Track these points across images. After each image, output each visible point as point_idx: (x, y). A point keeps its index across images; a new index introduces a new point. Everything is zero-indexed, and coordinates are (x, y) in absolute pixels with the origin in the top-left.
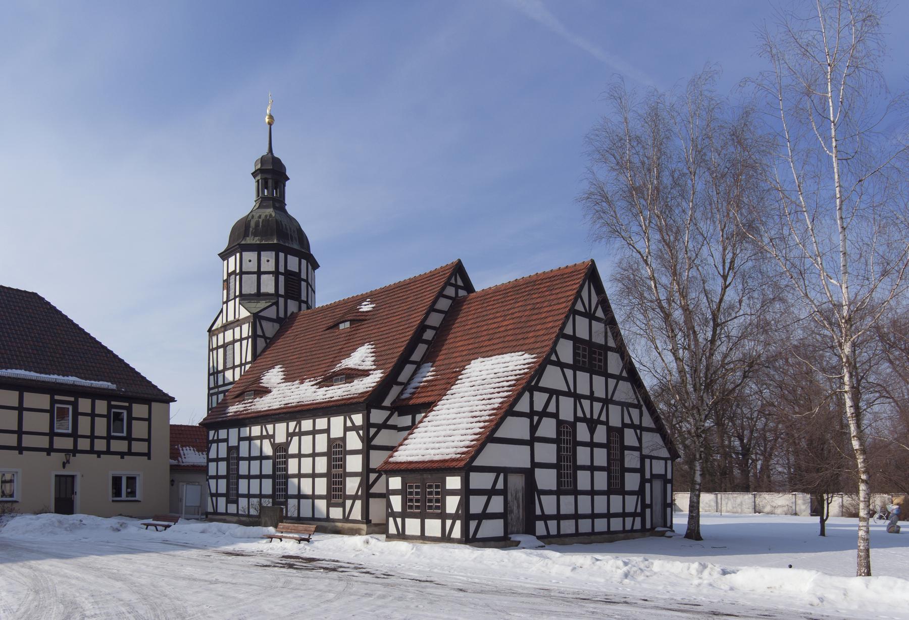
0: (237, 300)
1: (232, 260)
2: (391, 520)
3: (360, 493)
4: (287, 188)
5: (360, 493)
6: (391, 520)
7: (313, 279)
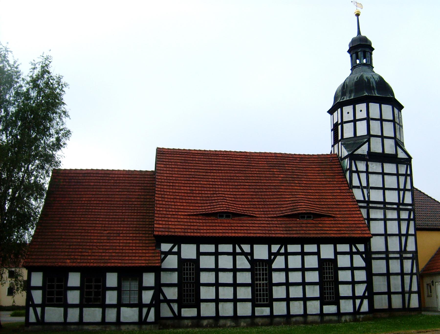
0: (340, 143)
1: (336, 114)
2: (31, 309)
3: (366, 294)
4: (373, 56)
5: (366, 294)
6: (31, 309)
7: (400, 118)
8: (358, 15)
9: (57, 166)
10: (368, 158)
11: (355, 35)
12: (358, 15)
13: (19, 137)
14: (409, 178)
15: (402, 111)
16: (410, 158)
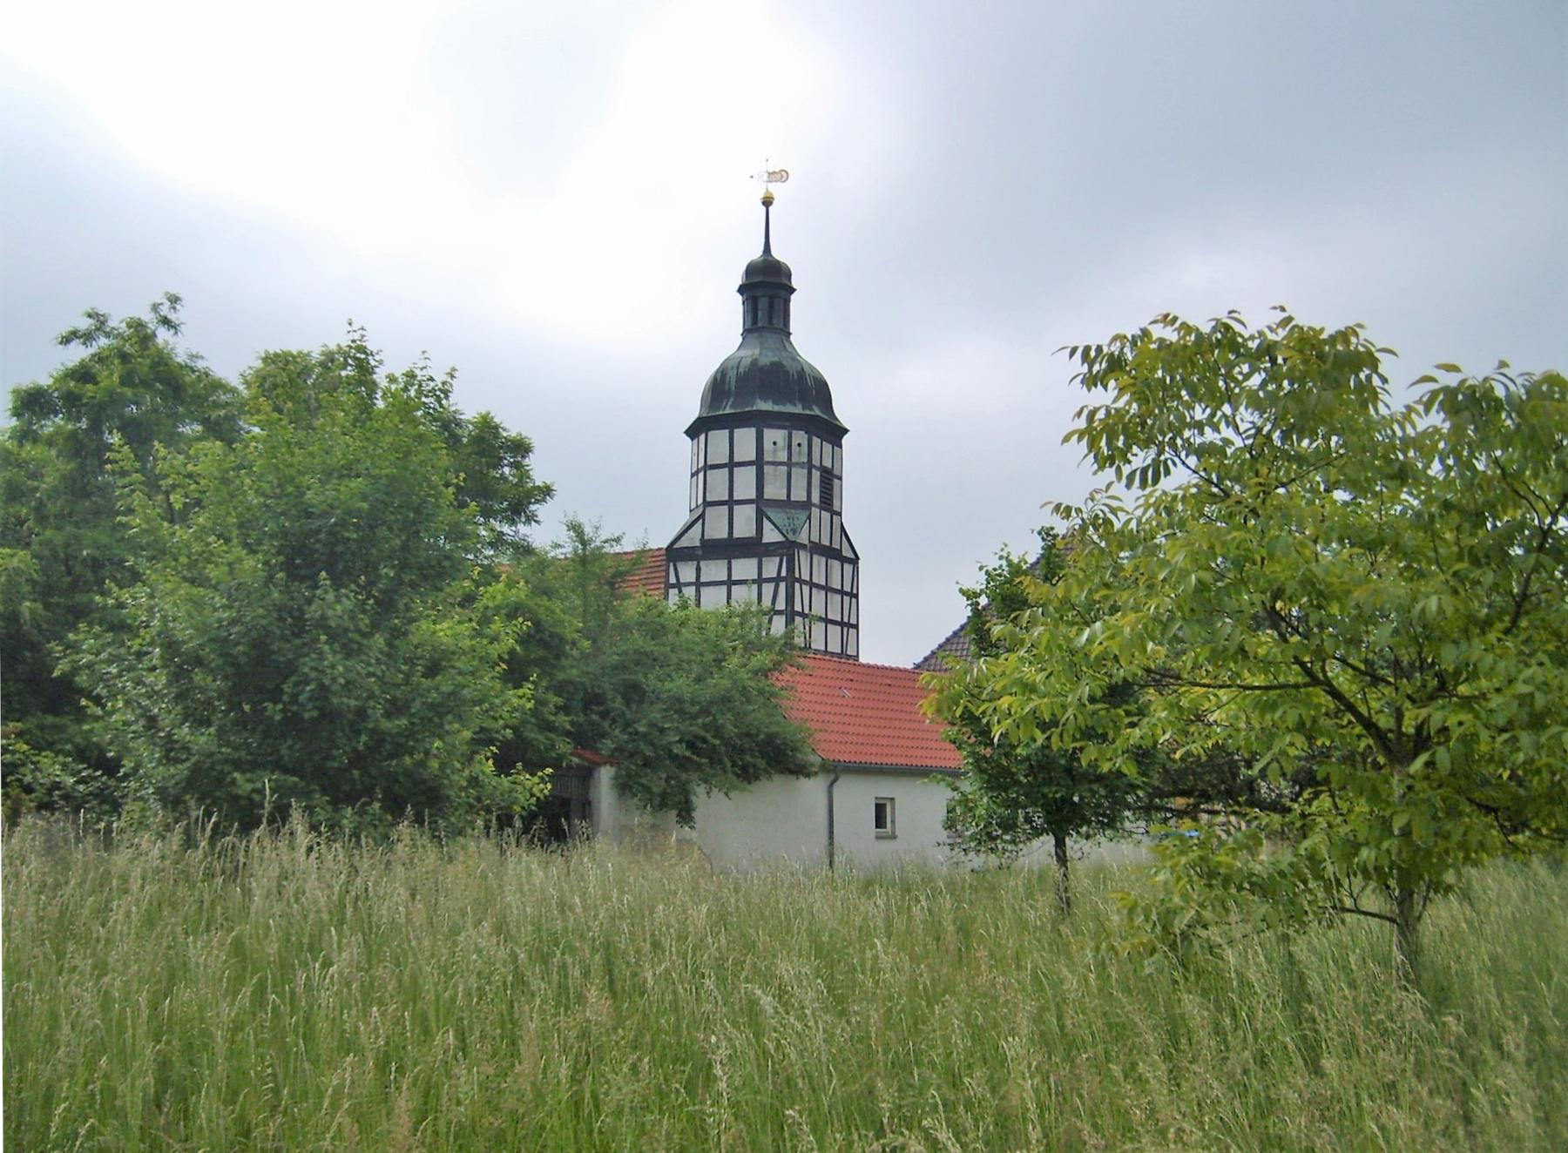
8: (767, 202)
9: (64, 732)
10: (700, 552)
11: (756, 253)
12: (767, 202)
13: (1460, 397)
14: (854, 600)
15: (843, 441)
16: (858, 558)
